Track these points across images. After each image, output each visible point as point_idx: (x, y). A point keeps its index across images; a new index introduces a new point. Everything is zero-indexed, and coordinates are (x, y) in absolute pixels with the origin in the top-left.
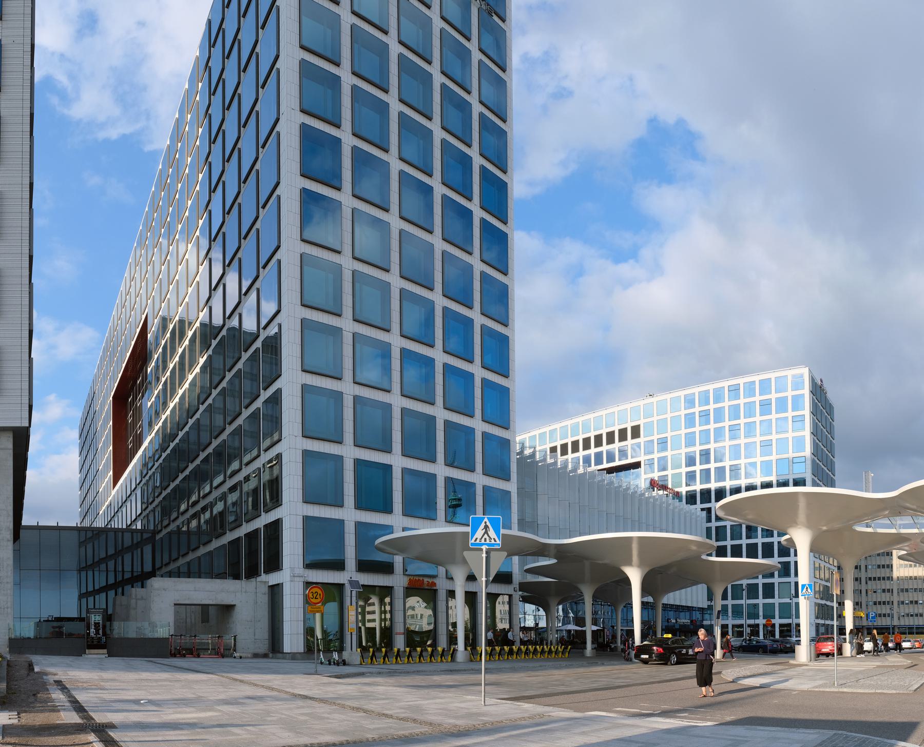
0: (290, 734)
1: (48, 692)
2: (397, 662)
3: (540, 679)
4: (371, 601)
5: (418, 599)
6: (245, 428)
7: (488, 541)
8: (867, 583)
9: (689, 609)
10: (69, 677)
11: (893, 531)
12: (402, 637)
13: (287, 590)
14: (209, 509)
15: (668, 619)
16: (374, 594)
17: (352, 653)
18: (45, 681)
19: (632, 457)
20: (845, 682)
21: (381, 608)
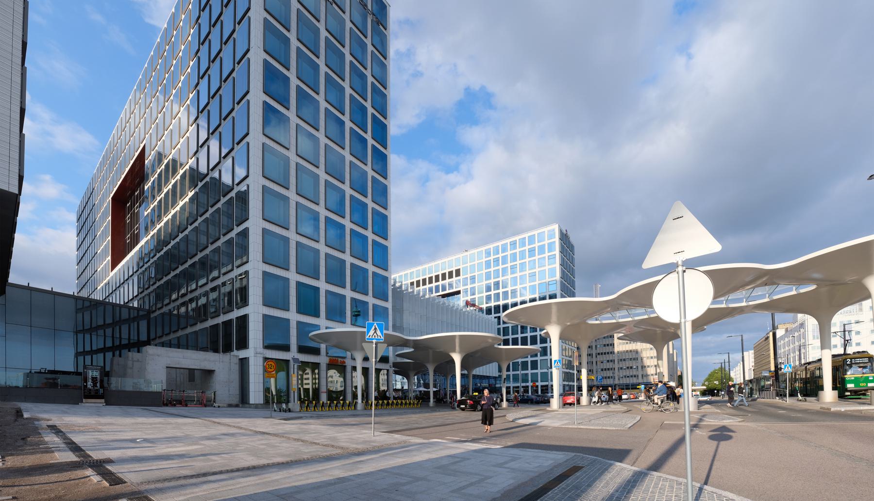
0: (253, 458)
1: (41, 436)
2: (322, 410)
3: (404, 420)
4: (306, 372)
5: (334, 371)
6: (223, 249)
7: (376, 337)
8: (596, 357)
9: (488, 377)
10: (64, 422)
11: (614, 321)
12: (325, 394)
13: (252, 362)
14: (195, 301)
15: (476, 384)
16: (308, 367)
17: (295, 404)
18: (37, 426)
19: (456, 288)
20: (581, 422)
21: (313, 376)
